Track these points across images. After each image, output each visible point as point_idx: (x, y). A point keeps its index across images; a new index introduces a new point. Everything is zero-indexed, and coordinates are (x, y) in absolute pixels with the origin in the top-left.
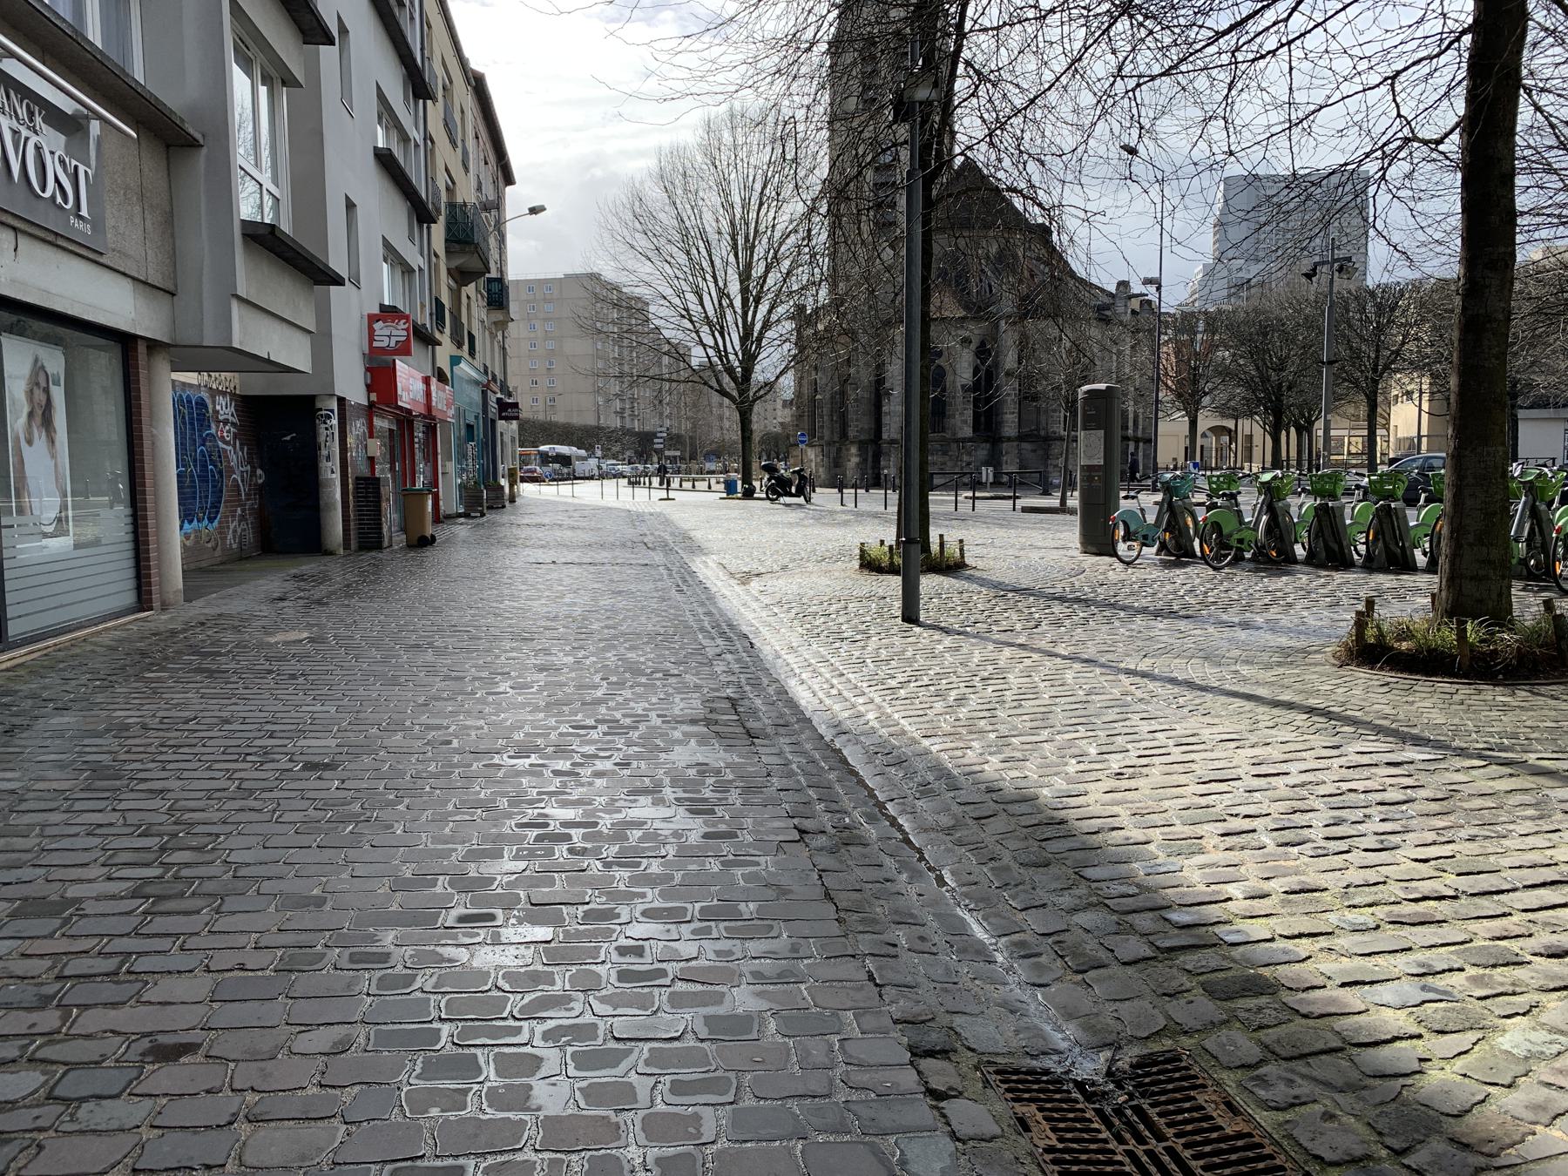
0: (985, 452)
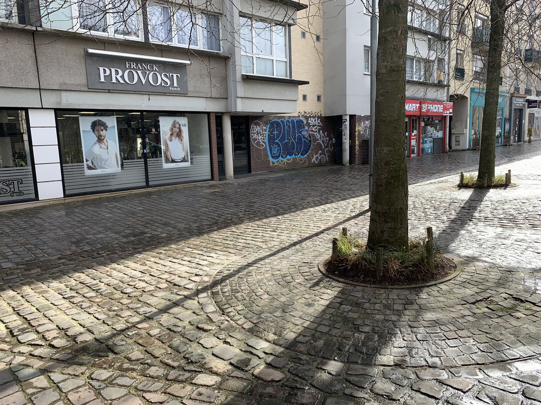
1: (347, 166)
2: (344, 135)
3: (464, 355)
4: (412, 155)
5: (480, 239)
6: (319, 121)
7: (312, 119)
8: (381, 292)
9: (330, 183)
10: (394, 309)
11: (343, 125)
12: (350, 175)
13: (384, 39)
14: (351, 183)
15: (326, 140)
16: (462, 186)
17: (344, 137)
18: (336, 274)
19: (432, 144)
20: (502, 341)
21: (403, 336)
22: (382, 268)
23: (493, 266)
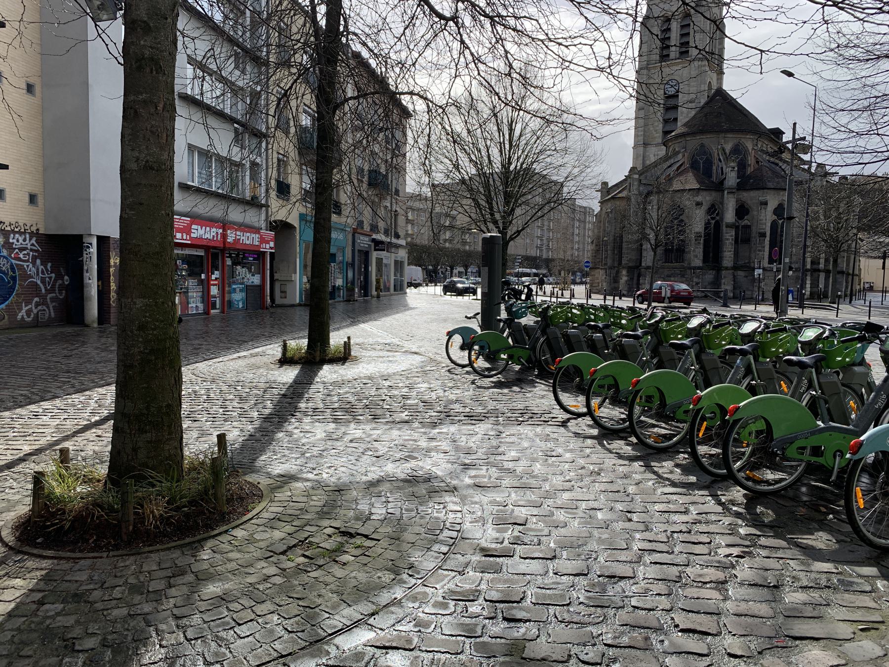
0: (712, 276)
1: (94, 328)
2: (87, 271)
3: (261, 647)
4: (212, 311)
5: (303, 445)
6: (33, 241)
7: (17, 236)
8: (127, 563)
9: (55, 359)
10: (148, 591)
11: (85, 252)
12: (98, 345)
13: (132, 111)
14: (98, 359)
15: (50, 278)
16: (285, 361)
17: (86, 275)
18: (39, 543)
19: (244, 294)
20: (320, 608)
21: (160, 640)
22: (132, 518)
23: (319, 485)
